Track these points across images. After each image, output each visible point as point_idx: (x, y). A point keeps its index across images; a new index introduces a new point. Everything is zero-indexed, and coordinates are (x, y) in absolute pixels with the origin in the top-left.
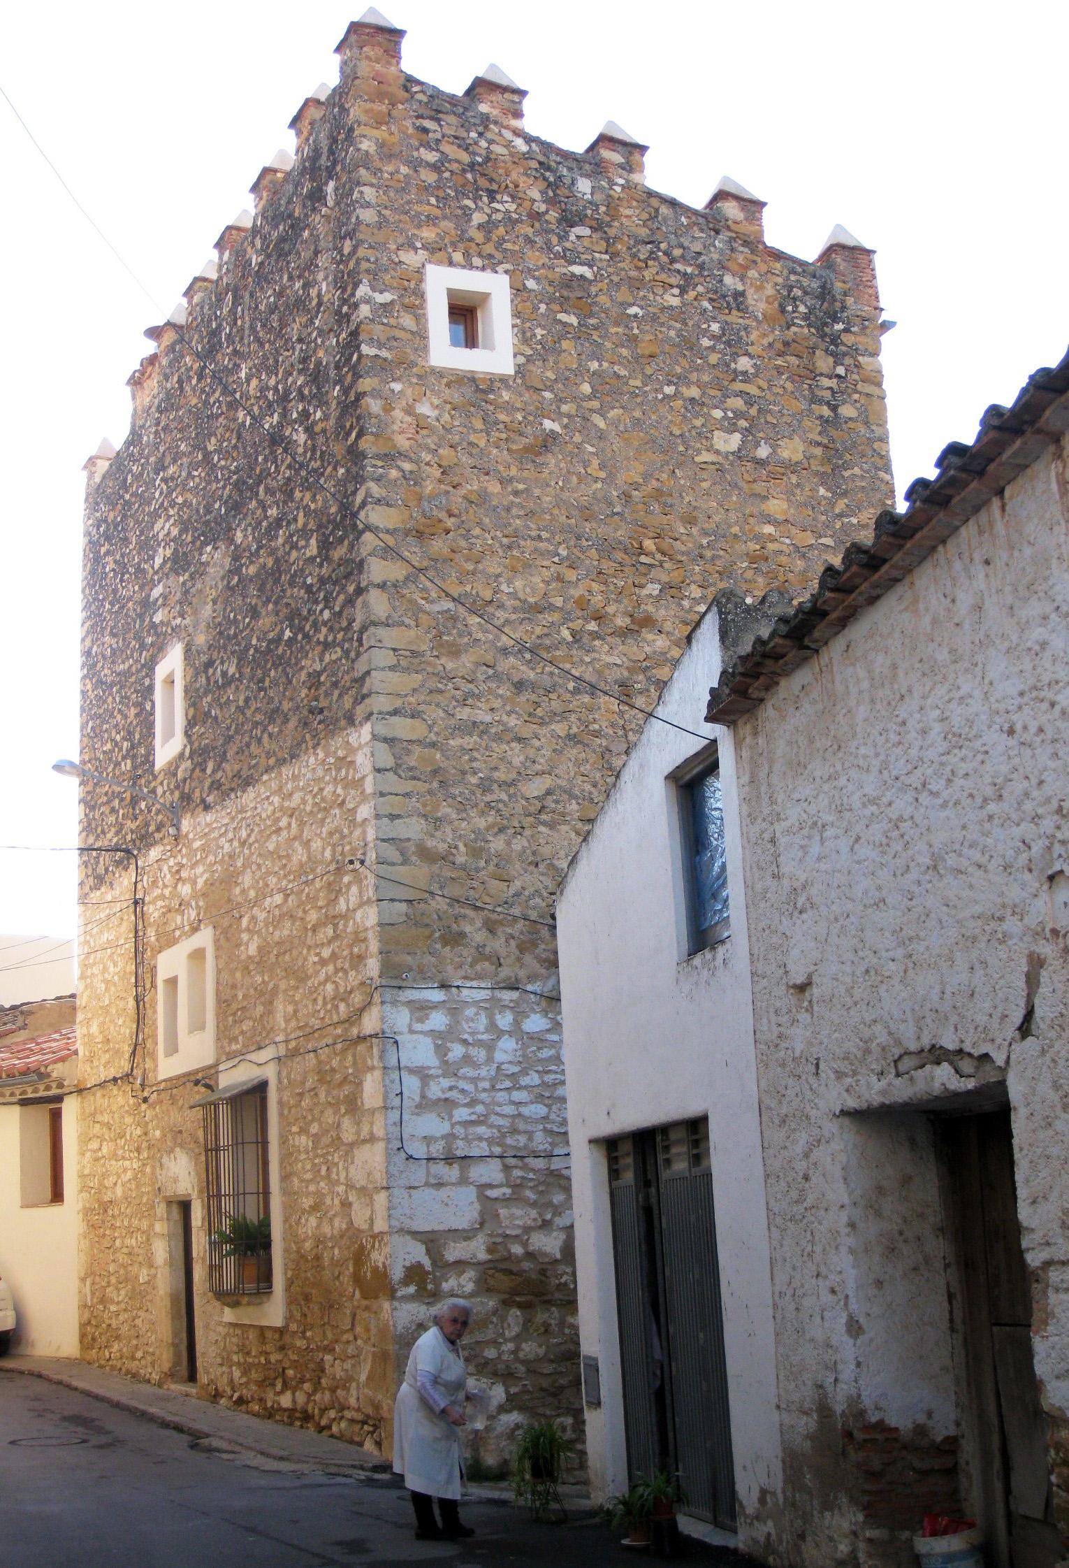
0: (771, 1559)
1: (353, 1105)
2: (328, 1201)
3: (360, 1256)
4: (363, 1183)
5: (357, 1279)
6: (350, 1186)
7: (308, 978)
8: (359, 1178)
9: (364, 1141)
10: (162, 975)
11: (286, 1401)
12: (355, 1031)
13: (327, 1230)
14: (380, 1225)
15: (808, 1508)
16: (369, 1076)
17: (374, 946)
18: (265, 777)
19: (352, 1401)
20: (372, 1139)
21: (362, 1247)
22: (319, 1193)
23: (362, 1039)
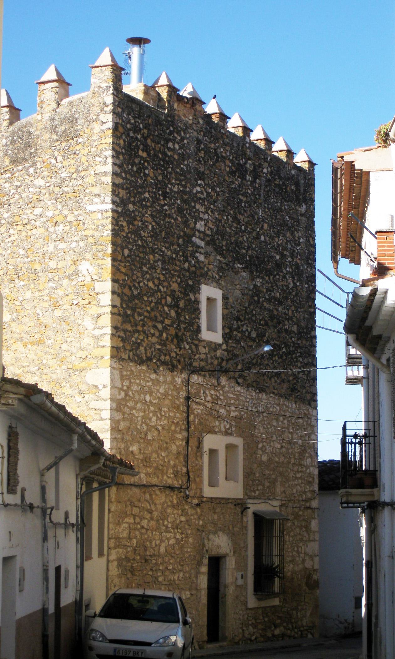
0: (184, 428)
1: (307, 528)
2: (297, 559)
3: (309, 577)
4: (311, 553)
5: (307, 584)
6: (306, 554)
7: (249, 423)
8: (310, 552)
9: (312, 541)
10: (206, 448)
11: (277, 632)
12: (308, 505)
13: (296, 568)
14: (316, 567)
15: (67, 104)
16: (313, 521)
17: (317, 481)
18: (272, 395)
19: (304, 624)
20: (314, 540)
21: (310, 574)
22: (293, 556)
23: (309, 508)
